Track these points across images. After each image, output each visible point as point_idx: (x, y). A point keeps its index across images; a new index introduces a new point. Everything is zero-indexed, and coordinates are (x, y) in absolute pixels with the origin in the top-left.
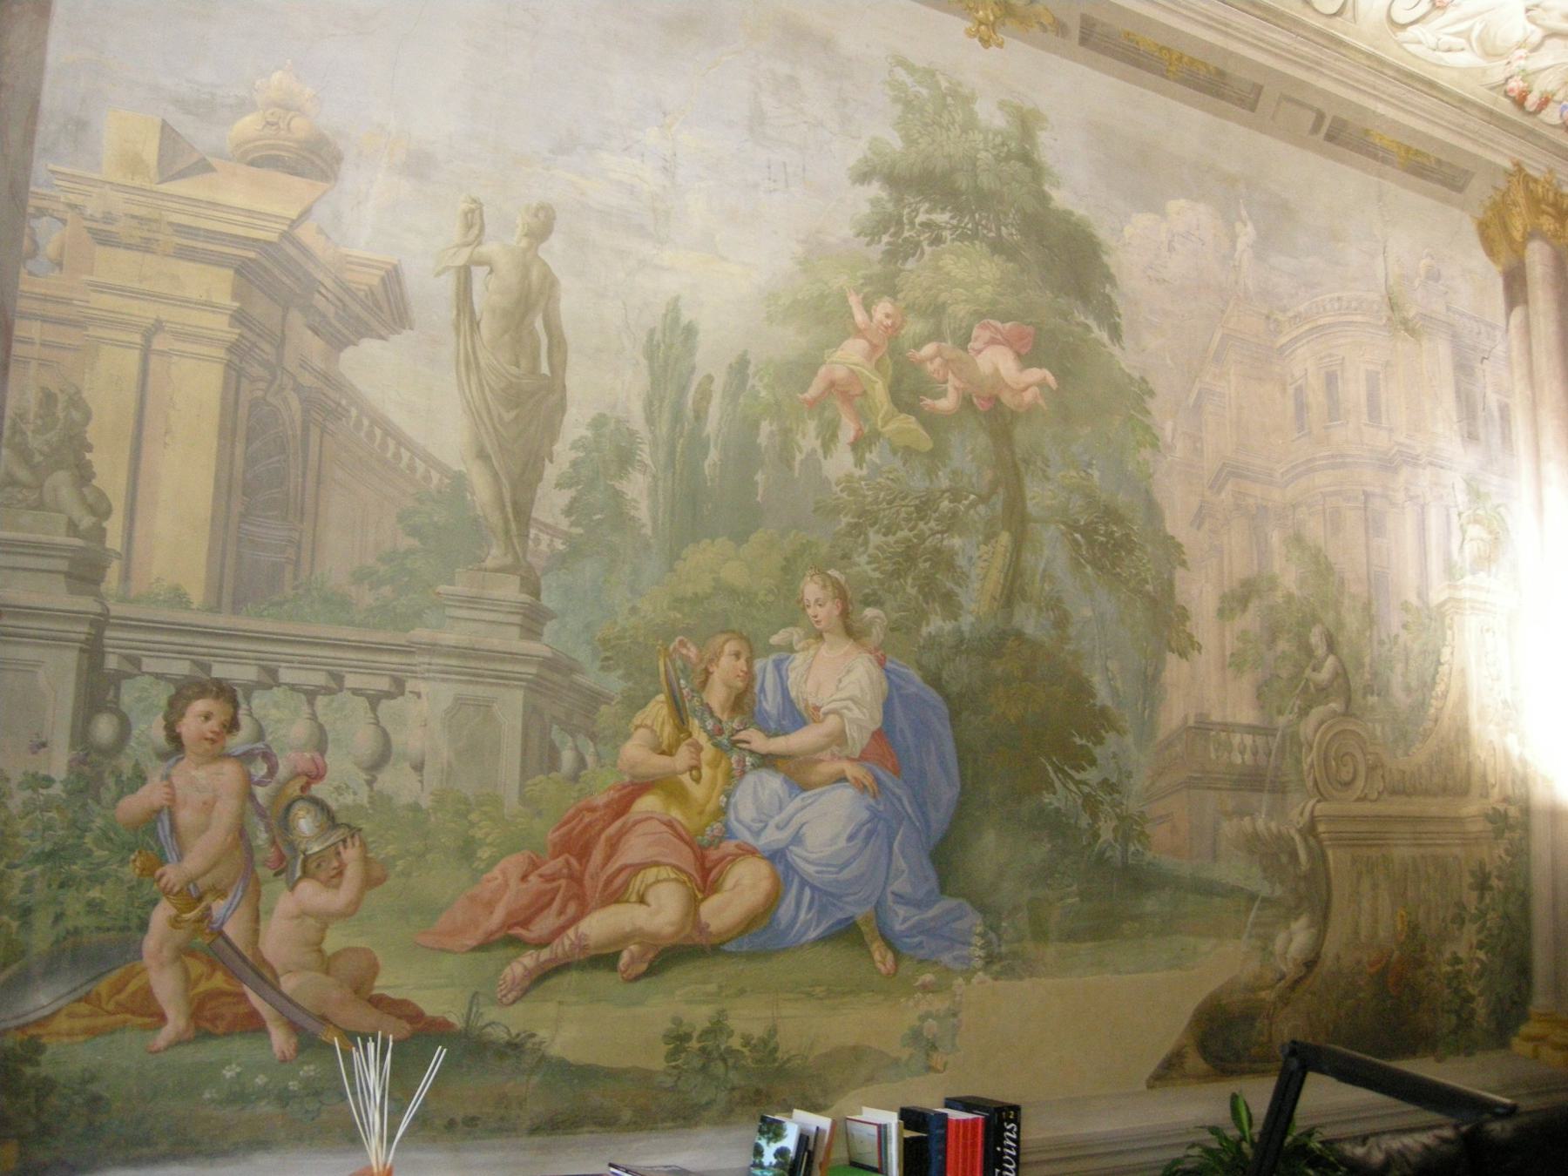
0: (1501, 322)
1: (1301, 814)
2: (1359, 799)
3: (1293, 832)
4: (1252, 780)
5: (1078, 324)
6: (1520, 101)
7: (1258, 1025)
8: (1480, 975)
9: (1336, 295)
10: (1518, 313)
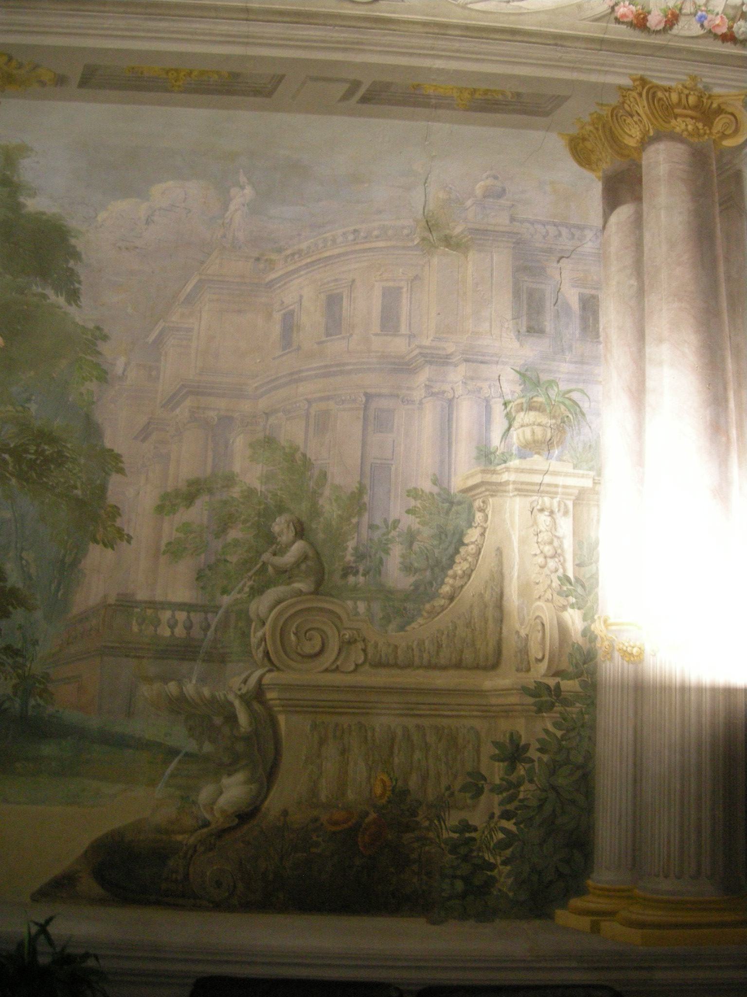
0: (598, 222)
1: (245, 682)
2: (326, 670)
3: (231, 697)
4: (185, 650)
5: (34, 295)
6: (640, 23)
7: (171, 863)
8: (503, 845)
9: (352, 228)
10: (624, 212)
